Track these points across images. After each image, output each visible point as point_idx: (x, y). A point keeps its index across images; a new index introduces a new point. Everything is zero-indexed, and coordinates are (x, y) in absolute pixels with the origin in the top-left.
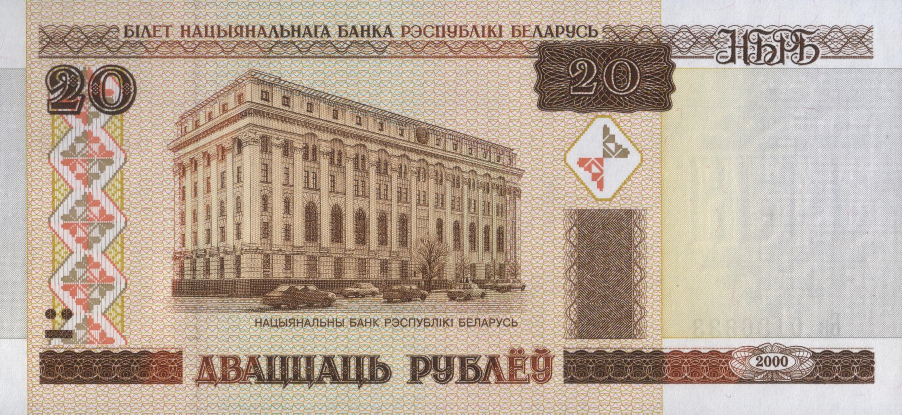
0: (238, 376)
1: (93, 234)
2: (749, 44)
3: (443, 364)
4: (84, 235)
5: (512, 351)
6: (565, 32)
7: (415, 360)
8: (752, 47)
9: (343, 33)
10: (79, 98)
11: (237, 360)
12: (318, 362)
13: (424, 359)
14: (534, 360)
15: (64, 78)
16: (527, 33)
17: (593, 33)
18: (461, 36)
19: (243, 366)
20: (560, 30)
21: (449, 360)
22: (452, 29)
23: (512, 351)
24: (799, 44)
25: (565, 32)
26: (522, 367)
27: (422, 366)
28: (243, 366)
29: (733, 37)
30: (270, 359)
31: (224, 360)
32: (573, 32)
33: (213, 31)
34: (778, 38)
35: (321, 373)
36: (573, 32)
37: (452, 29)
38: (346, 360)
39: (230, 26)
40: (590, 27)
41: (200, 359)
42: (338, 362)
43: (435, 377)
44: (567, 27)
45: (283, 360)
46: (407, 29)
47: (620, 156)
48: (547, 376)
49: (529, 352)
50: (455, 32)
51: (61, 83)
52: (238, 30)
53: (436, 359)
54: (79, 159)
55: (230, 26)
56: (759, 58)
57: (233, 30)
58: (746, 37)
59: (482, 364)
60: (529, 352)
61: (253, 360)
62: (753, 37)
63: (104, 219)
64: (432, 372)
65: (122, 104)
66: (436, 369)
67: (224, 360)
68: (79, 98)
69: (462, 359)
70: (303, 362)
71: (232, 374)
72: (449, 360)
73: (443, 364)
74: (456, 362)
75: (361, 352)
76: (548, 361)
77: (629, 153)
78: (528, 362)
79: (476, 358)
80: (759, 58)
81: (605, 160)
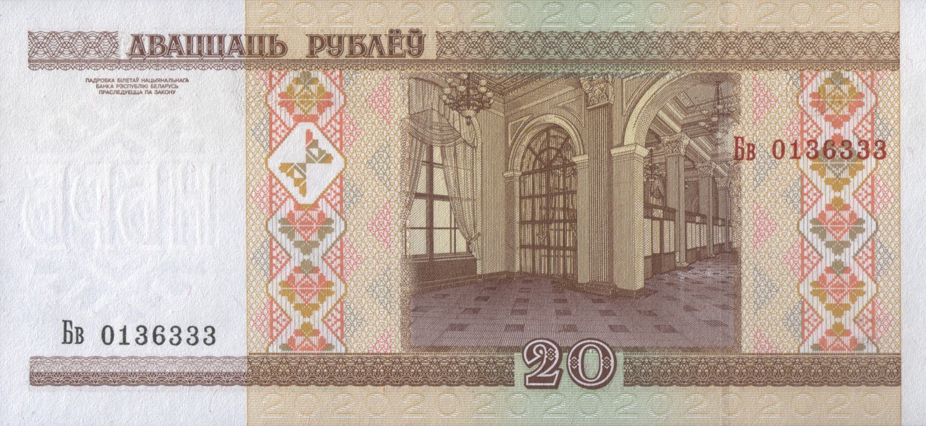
0: (163, 51)
1: (843, 176)
3: (335, 42)
4: (841, 212)
5: (391, 31)
7: (312, 38)
10: (557, 372)
11: (162, 38)
12: (228, 41)
13: (321, 38)
14: (409, 39)
15: (541, 352)
19: (167, 43)
21: (340, 39)
23: (391, 31)
26: (400, 44)
27: (318, 43)
28: (167, 43)
30: (189, 38)
31: (152, 38)
35: (231, 49)
38: (250, 39)
41: (132, 38)
42: (244, 40)
43: (329, 52)
45: (261, 39)
47: (323, 161)
48: (339, 52)
49: (405, 32)
51: (539, 356)
53: (329, 38)
54: (315, 226)
59: (367, 42)
60: (405, 32)
61: (175, 38)
63: (854, 97)
64: (327, 48)
66: (330, 45)
67: (152, 38)
68: (557, 372)
69: (351, 38)
70: (216, 40)
71: (159, 50)
72: (340, 39)
73: (335, 42)
74: (346, 41)
75: (211, 33)
76: (421, 40)
77: (280, 168)
78: (405, 40)
79: (363, 37)
81: (308, 165)
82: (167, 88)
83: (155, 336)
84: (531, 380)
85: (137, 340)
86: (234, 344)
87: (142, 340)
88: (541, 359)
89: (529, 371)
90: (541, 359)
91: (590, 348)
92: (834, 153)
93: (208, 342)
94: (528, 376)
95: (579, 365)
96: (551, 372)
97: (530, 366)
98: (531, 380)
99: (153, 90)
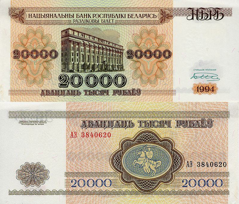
2: (199, 13)
6: (146, 16)
8: (198, 13)
9: (78, 17)
10: (68, 83)
15: (63, 77)
16: (133, 17)
17: (155, 17)
18: (112, 17)
20: (144, 15)
22: (109, 15)
24: (217, 13)
25: (146, 16)
29: (193, 10)
32: (148, 16)
33: (39, 16)
34: (209, 11)
36: (148, 16)
37: (109, 15)
39: (45, 14)
40: (154, 14)
44: (146, 14)
46: (94, 15)
50: (110, 16)
51: (63, 79)
52: (47, 15)
55: (45, 14)
56: (202, 18)
57: (46, 15)
58: (197, 11)
62: (200, 11)
65: (79, 85)
68: (68, 83)
80: (202, 18)
82: (42, 123)
83: (99, 135)
84: (61, 85)
85: (82, 136)
86: (178, 21)
87: (83, 136)
88: (63, 79)
89: (60, 82)
90: (63, 79)
91: (90, 77)
92: (217, 165)
93: (198, 166)
94: (60, 84)
95: (117, 81)
96: (66, 83)
97: (60, 81)
98: (61, 85)
99: (34, 124)
